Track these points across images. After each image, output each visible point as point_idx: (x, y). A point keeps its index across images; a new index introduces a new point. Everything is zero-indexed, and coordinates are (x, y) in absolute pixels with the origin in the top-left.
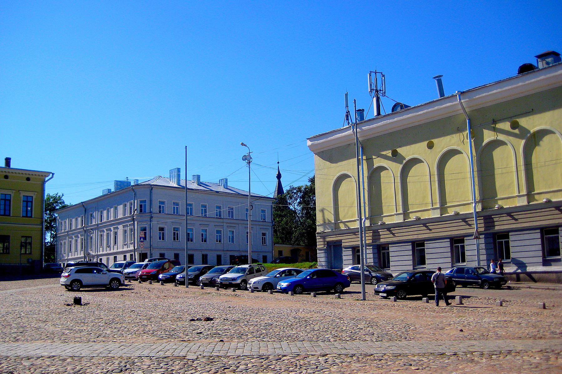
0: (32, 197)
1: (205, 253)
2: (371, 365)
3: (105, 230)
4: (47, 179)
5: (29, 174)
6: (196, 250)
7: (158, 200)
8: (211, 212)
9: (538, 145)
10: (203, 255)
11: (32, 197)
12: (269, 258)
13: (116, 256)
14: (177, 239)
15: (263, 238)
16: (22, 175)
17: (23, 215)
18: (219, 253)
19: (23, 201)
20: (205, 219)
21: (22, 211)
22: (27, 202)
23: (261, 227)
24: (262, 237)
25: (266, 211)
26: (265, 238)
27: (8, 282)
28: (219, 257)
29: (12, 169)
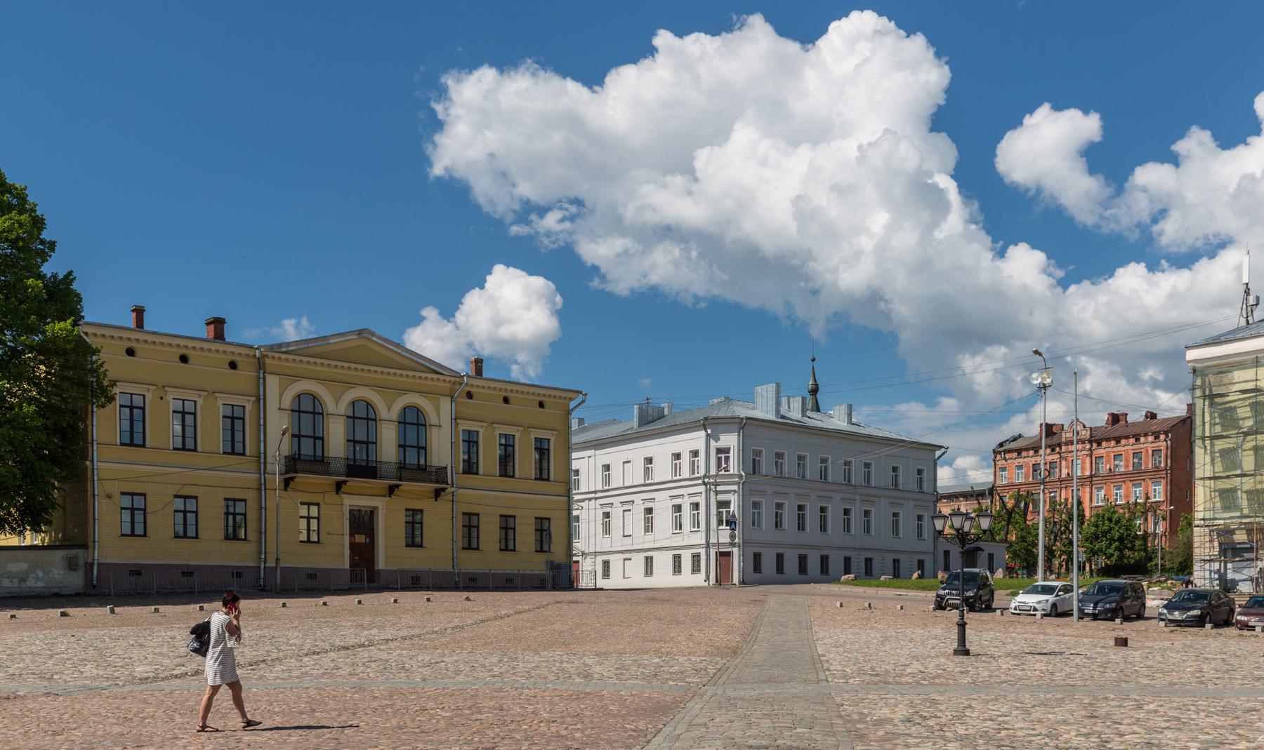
0: (244, 407)
1: (824, 552)
2: (602, 736)
3: (616, 501)
4: (572, 404)
5: (186, 347)
6: (902, 552)
7: (764, 449)
8: (835, 474)
9: (847, 16)
10: (822, 557)
11: (244, 407)
13: (651, 558)
14: (781, 526)
15: (799, 514)
16: (488, 391)
17: (227, 451)
18: (848, 554)
19: (224, 417)
20: (869, 491)
21: (221, 441)
22: (233, 418)
23: (865, 498)
24: (775, 510)
25: (808, 459)
26: (781, 513)
27: (543, 595)
28: (847, 560)
29: (487, 379)
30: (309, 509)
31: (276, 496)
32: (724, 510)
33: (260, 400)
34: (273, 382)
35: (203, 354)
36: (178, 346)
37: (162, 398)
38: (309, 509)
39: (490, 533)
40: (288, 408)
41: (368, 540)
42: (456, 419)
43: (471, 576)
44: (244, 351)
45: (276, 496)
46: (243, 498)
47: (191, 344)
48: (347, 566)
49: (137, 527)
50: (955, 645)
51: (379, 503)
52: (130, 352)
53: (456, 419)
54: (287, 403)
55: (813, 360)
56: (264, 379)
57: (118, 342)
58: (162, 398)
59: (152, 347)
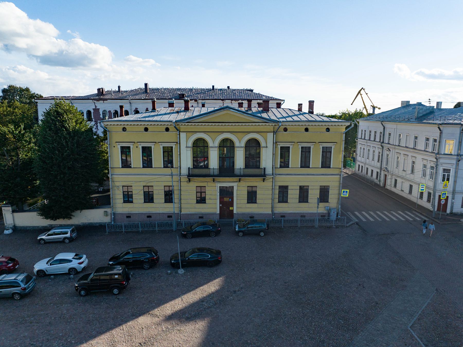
12: (453, 200)
30: (128, 190)
31: (184, 184)
32: (446, 174)
33: (178, 143)
34: (183, 135)
35: (319, 127)
36: (325, 125)
37: (137, 147)
38: (128, 190)
39: (293, 194)
40: (190, 146)
41: (230, 200)
42: (276, 142)
43: (251, 215)
44: (169, 124)
45: (184, 184)
46: (204, 186)
47: (126, 123)
48: (218, 212)
49: (347, 192)
51: (235, 185)
52: (307, 130)
53: (276, 142)
54: (190, 144)
56: (179, 134)
57: (302, 127)
58: (137, 147)
59: (315, 127)
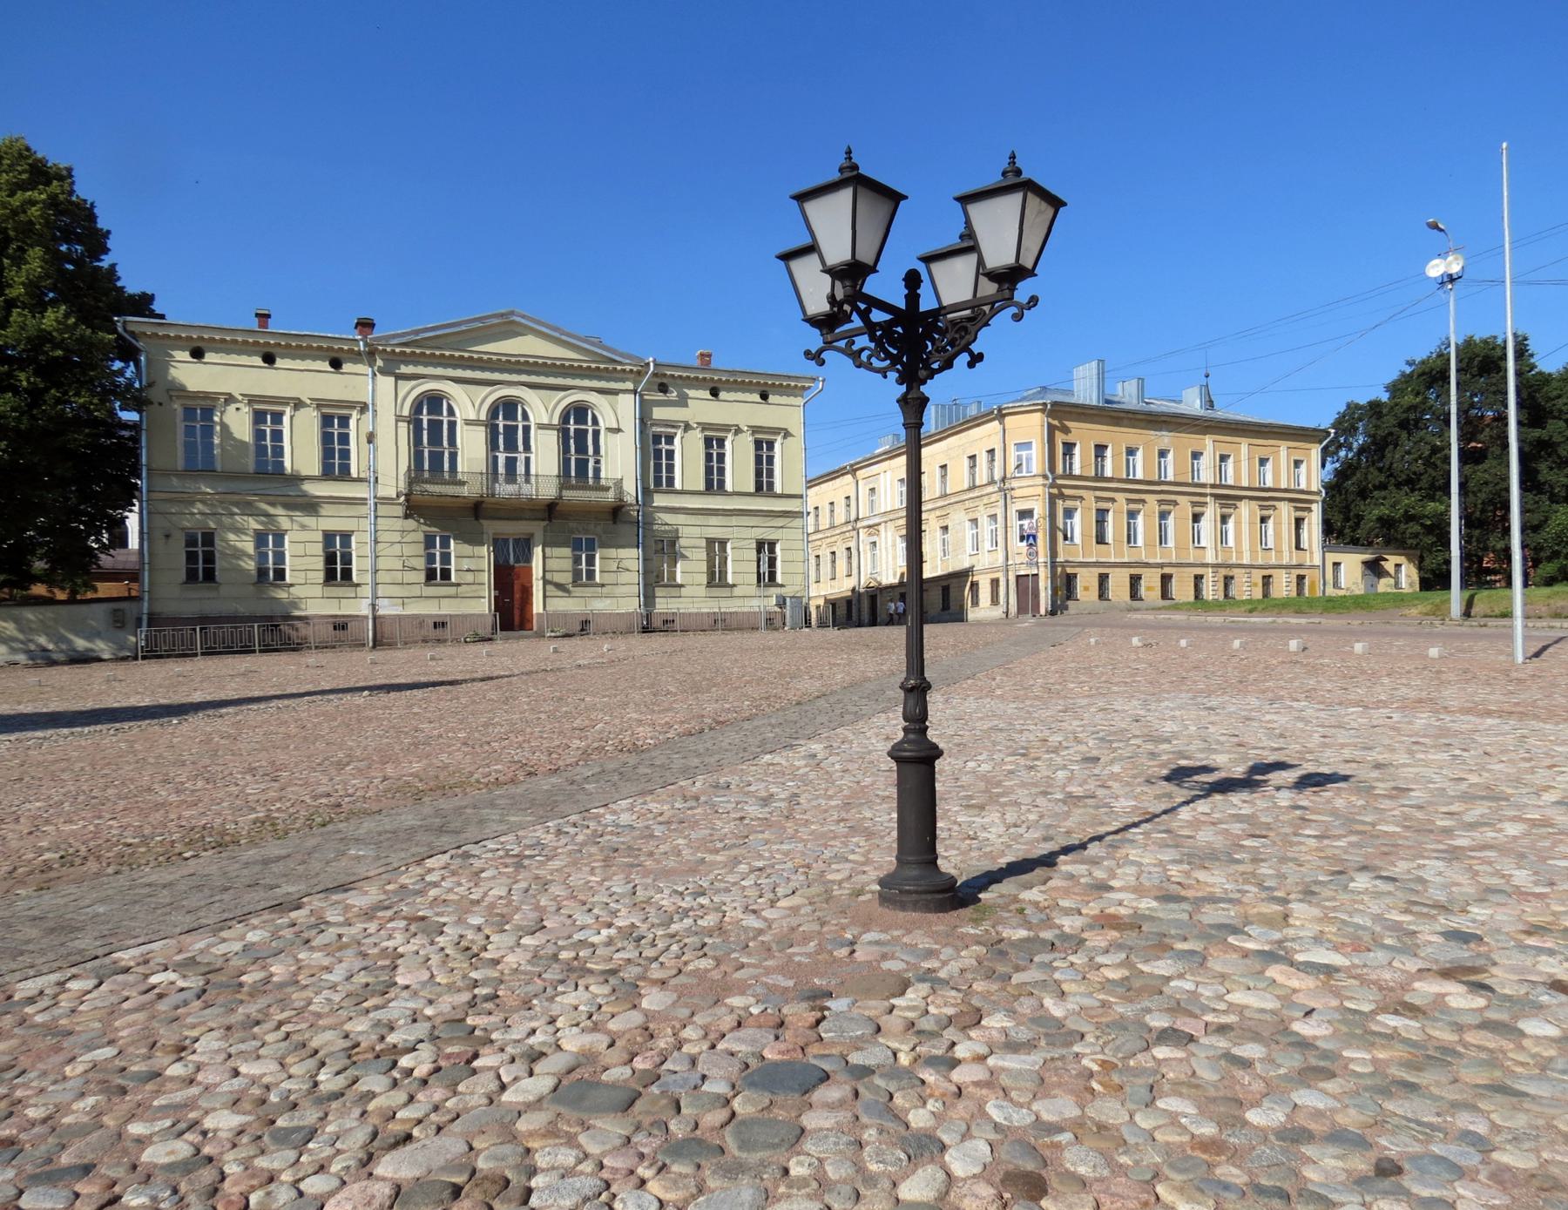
50: (885, 859)
55: (1207, 376)
